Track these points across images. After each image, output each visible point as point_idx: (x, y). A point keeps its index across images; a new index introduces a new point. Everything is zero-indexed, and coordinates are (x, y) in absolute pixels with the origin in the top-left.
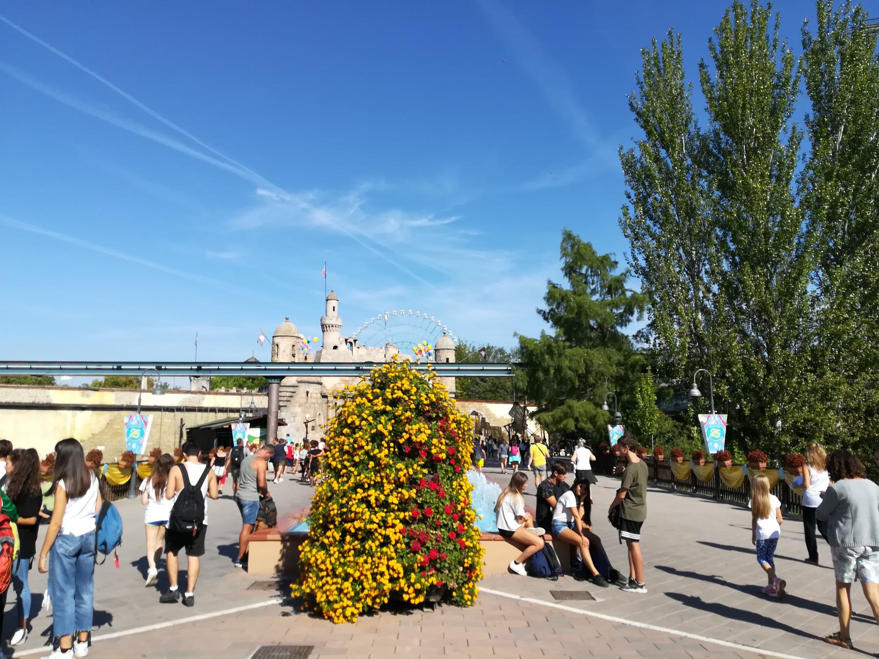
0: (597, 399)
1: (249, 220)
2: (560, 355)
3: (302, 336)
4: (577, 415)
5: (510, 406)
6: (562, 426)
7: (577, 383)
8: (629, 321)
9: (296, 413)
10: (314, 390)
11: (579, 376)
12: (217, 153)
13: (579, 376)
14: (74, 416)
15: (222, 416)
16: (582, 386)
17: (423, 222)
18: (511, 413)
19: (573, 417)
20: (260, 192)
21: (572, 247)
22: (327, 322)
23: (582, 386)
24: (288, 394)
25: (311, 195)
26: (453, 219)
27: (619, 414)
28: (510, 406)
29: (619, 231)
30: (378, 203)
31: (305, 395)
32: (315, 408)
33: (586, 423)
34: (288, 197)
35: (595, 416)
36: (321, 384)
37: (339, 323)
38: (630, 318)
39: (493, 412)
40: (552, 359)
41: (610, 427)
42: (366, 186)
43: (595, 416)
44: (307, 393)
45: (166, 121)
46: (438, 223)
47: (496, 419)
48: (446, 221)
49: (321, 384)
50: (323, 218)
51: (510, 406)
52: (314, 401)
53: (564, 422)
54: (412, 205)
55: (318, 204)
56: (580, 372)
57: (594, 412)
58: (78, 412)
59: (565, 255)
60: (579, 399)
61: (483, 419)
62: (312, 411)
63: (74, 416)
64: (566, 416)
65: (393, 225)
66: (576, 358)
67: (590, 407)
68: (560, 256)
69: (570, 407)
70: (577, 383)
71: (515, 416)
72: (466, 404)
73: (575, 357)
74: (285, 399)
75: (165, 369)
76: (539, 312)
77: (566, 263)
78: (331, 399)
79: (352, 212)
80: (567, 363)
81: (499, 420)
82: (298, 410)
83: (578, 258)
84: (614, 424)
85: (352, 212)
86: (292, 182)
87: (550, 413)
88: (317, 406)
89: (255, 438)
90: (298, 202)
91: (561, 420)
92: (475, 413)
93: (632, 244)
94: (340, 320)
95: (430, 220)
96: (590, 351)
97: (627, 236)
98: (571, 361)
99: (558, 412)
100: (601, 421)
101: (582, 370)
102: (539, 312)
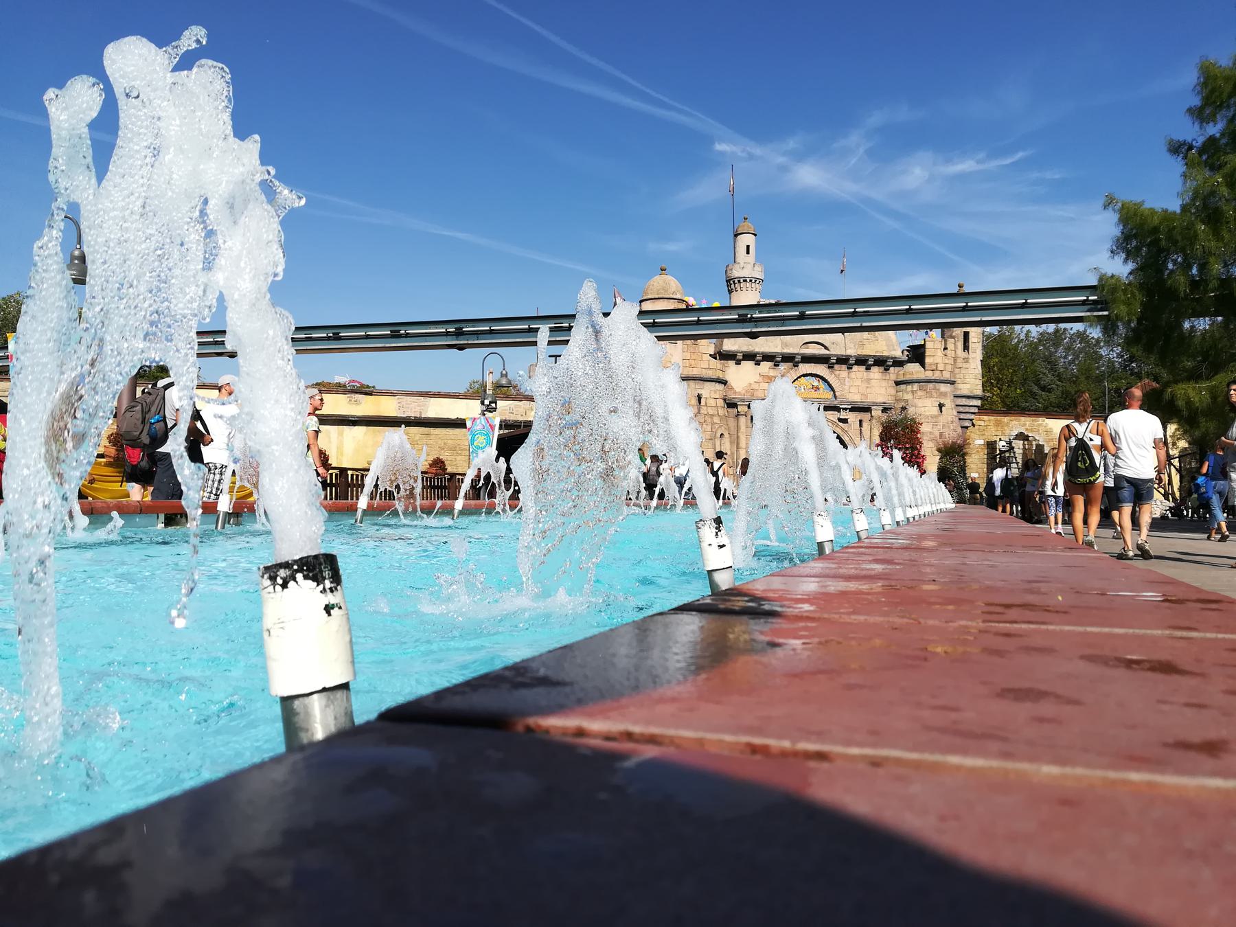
1: (706, 191)
14: (341, 434)
17: (966, 165)
20: (719, 147)
22: (737, 273)
25: (792, 144)
26: (1020, 155)
30: (897, 143)
32: (713, 424)
34: (758, 151)
36: (724, 383)
37: (758, 273)
40: (1217, 234)
42: (876, 119)
44: (699, 397)
46: (993, 164)
48: (1008, 161)
50: (810, 176)
52: (711, 411)
54: (946, 139)
55: (800, 156)
62: (709, 428)
63: (341, 434)
65: (917, 175)
72: (1006, 419)
75: (407, 335)
76: (1177, 148)
86: (760, 125)
88: (716, 420)
90: (771, 155)
94: (758, 268)
95: (978, 162)
102: (1177, 148)
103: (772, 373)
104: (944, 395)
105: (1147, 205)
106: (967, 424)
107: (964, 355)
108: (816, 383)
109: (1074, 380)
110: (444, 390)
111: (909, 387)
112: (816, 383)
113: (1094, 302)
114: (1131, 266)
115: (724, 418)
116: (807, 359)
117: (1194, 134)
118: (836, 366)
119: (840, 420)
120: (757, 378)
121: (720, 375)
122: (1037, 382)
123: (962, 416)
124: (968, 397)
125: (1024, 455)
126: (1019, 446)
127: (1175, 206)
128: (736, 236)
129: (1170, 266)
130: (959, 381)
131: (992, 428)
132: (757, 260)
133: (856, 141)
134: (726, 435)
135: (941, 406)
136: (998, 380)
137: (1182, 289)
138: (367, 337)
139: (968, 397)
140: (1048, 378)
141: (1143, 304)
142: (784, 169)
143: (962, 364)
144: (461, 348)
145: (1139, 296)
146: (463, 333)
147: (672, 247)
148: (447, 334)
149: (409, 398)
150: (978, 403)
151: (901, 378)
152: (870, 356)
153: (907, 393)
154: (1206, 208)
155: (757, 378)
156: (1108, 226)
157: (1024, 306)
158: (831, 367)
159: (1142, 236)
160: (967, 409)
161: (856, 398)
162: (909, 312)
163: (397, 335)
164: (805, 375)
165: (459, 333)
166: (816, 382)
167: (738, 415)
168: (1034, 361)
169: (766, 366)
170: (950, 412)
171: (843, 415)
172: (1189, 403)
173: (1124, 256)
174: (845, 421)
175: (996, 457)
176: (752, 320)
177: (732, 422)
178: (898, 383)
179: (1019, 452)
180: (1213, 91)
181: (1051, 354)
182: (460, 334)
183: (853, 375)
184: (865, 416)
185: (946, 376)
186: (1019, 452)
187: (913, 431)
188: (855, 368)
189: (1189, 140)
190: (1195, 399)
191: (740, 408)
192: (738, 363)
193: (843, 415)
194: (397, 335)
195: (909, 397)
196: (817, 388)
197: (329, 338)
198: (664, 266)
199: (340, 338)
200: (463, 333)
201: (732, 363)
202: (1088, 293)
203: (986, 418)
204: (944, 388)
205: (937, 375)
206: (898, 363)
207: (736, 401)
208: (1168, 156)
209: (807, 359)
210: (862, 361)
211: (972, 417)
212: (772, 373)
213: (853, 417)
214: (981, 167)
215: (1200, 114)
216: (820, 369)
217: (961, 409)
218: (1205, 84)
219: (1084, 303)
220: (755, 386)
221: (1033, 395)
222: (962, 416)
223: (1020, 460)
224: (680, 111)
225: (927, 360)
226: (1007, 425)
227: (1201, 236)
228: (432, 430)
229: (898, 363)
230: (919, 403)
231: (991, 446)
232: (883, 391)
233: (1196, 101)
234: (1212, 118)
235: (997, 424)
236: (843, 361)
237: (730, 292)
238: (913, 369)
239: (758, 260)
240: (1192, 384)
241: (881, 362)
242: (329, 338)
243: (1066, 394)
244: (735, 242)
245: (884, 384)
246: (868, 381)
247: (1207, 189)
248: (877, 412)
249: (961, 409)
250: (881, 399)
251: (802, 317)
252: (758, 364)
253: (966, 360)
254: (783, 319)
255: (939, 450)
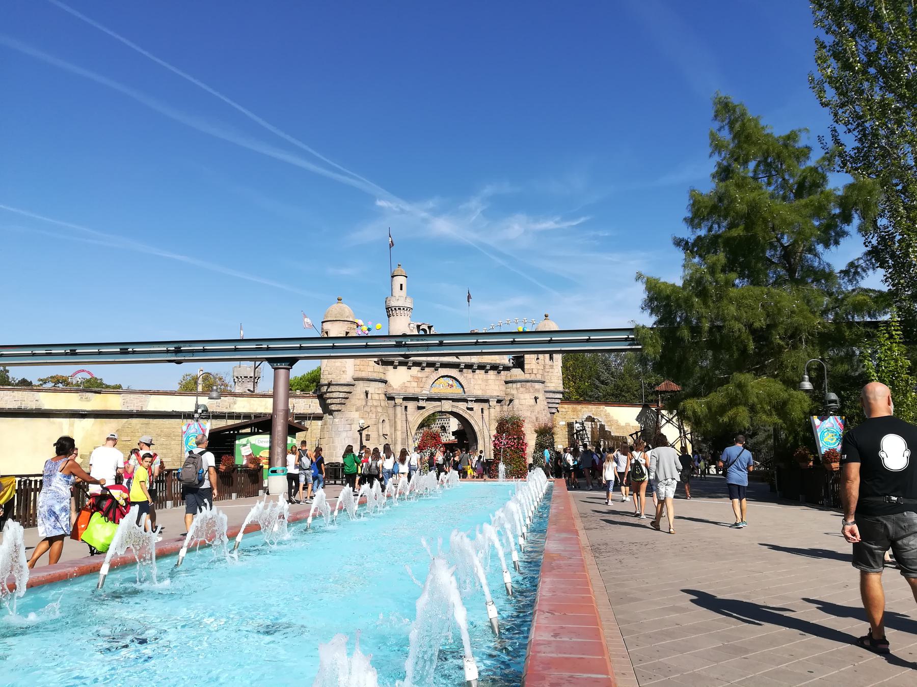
0: (789, 373)
1: (371, 233)
2: (720, 298)
3: (360, 322)
4: (753, 399)
5: (637, 410)
6: (726, 419)
7: (752, 346)
8: (844, 234)
9: (353, 420)
10: (376, 389)
11: (753, 331)
12: (337, 166)
13: (753, 331)
15: (231, 422)
16: (762, 349)
17: (549, 225)
18: (638, 419)
19: (746, 404)
20: (380, 203)
21: (731, 124)
22: (393, 303)
23: (762, 349)
24: (342, 395)
25: (431, 204)
26: (582, 220)
27: (833, 396)
28: (639, 410)
29: (811, 96)
30: (502, 208)
31: (363, 396)
32: (377, 412)
33: (769, 414)
34: (407, 207)
35: (785, 403)
36: (385, 382)
38: (846, 228)
39: (615, 418)
40: (705, 303)
41: (816, 421)
42: (488, 190)
43: (785, 403)
44: (367, 393)
45: (288, 137)
47: (619, 427)
49: (385, 382)
51: (637, 410)
52: (375, 404)
53: (730, 413)
54: (535, 207)
56: (757, 325)
57: (784, 395)
58: (77, 421)
59: (718, 147)
60: (759, 372)
61: (602, 427)
63: (72, 425)
64: (733, 402)
65: (516, 230)
66: (749, 301)
67: (777, 387)
68: (709, 150)
69: (740, 386)
70: (752, 346)
71: (645, 423)
72: (579, 407)
73: (745, 301)
74: (338, 401)
75: (134, 352)
76: (678, 243)
77: (719, 164)
78: (399, 401)
79: (474, 218)
80: (732, 309)
81: (622, 428)
82: (355, 415)
83: (741, 140)
84: (823, 416)
85: (474, 218)
86: (408, 191)
87: (703, 400)
88: (379, 410)
89: (263, 448)
90: (417, 211)
91: (723, 410)
92: (591, 419)
93: (836, 115)
95: (556, 223)
96: (774, 290)
97: (824, 105)
98: (739, 308)
99: (717, 397)
100: (796, 413)
101: (761, 323)
102: (678, 243)
103: (420, 375)
104: (538, 391)
105: (662, 280)
106: (554, 410)
107: (550, 363)
108: (451, 382)
109: (622, 377)
110: (161, 389)
111: (514, 385)
112: (451, 382)
113: (633, 339)
114: (654, 319)
115: (385, 408)
116: (445, 365)
117: (689, 235)
118: (465, 370)
119: (468, 409)
120: (409, 379)
121: (382, 377)
122: (598, 379)
123: (551, 405)
124: (554, 392)
125: (593, 432)
126: (588, 425)
127: (679, 283)
128: (393, 277)
129: (678, 320)
130: (547, 381)
131: (570, 413)
132: (408, 294)
133: (475, 204)
134: (387, 421)
135: (536, 398)
136: (573, 376)
137: (686, 338)
138: (100, 353)
139: (554, 392)
140: (605, 376)
141: (663, 347)
142: (425, 221)
143: (550, 371)
144: (179, 362)
145: (660, 341)
146: (181, 351)
147: (345, 271)
148: (168, 351)
149: (132, 396)
150: (561, 396)
151: (509, 379)
152: (488, 364)
153: (513, 389)
154: (697, 285)
155: (409, 379)
156: (640, 293)
157: (588, 341)
158: (461, 371)
159: (659, 299)
160: (553, 401)
161: (479, 393)
162: (513, 343)
163: (125, 351)
164: (443, 377)
165: (178, 351)
166: (450, 381)
167: (395, 405)
168: (595, 363)
169: (415, 370)
170: (542, 402)
171: (470, 405)
172: (694, 412)
173: (649, 311)
174: (471, 409)
175: (573, 435)
176: (406, 345)
177: (391, 411)
178: (506, 382)
179: (589, 430)
180: (698, 209)
181: (606, 359)
182: (178, 351)
183: (476, 376)
184: (485, 405)
185: (539, 377)
186: (589, 430)
187: (518, 426)
188: (478, 371)
189: (686, 238)
190: (698, 410)
191: (397, 401)
192: (395, 368)
193: (470, 405)
194: (125, 351)
195: (514, 392)
196: (452, 386)
197: (66, 354)
198: (340, 297)
199: (76, 354)
200: (181, 351)
201: (391, 367)
202: (628, 333)
203: (566, 406)
204: (537, 386)
205: (533, 377)
206: (507, 368)
207: (393, 395)
208: (673, 247)
209: (445, 365)
210: (482, 367)
211: (557, 406)
212: (420, 375)
213: (477, 407)
214: (557, 226)
215: (693, 222)
216: (453, 372)
217: (549, 401)
218: (693, 205)
219: (626, 340)
220: (408, 384)
221: (597, 387)
222: (551, 405)
223: (589, 436)
224: (352, 177)
225: (526, 367)
226: (580, 411)
227: (696, 305)
228: (151, 421)
229: (507, 368)
230: (522, 396)
231: (570, 426)
232: (497, 388)
233: (689, 215)
234: (699, 226)
235: (574, 411)
236: (469, 366)
237: (389, 316)
238: (516, 373)
239: (409, 294)
240: (696, 400)
241: (495, 367)
242: (66, 354)
243: (617, 387)
244: (392, 281)
245: (497, 383)
246: (487, 380)
247: (698, 275)
248: (493, 403)
249: (549, 401)
250: (495, 394)
251: (441, 344)
252: (409, 368)
253: (552, 367)
254: (428, 345)
255: (536, 431)
